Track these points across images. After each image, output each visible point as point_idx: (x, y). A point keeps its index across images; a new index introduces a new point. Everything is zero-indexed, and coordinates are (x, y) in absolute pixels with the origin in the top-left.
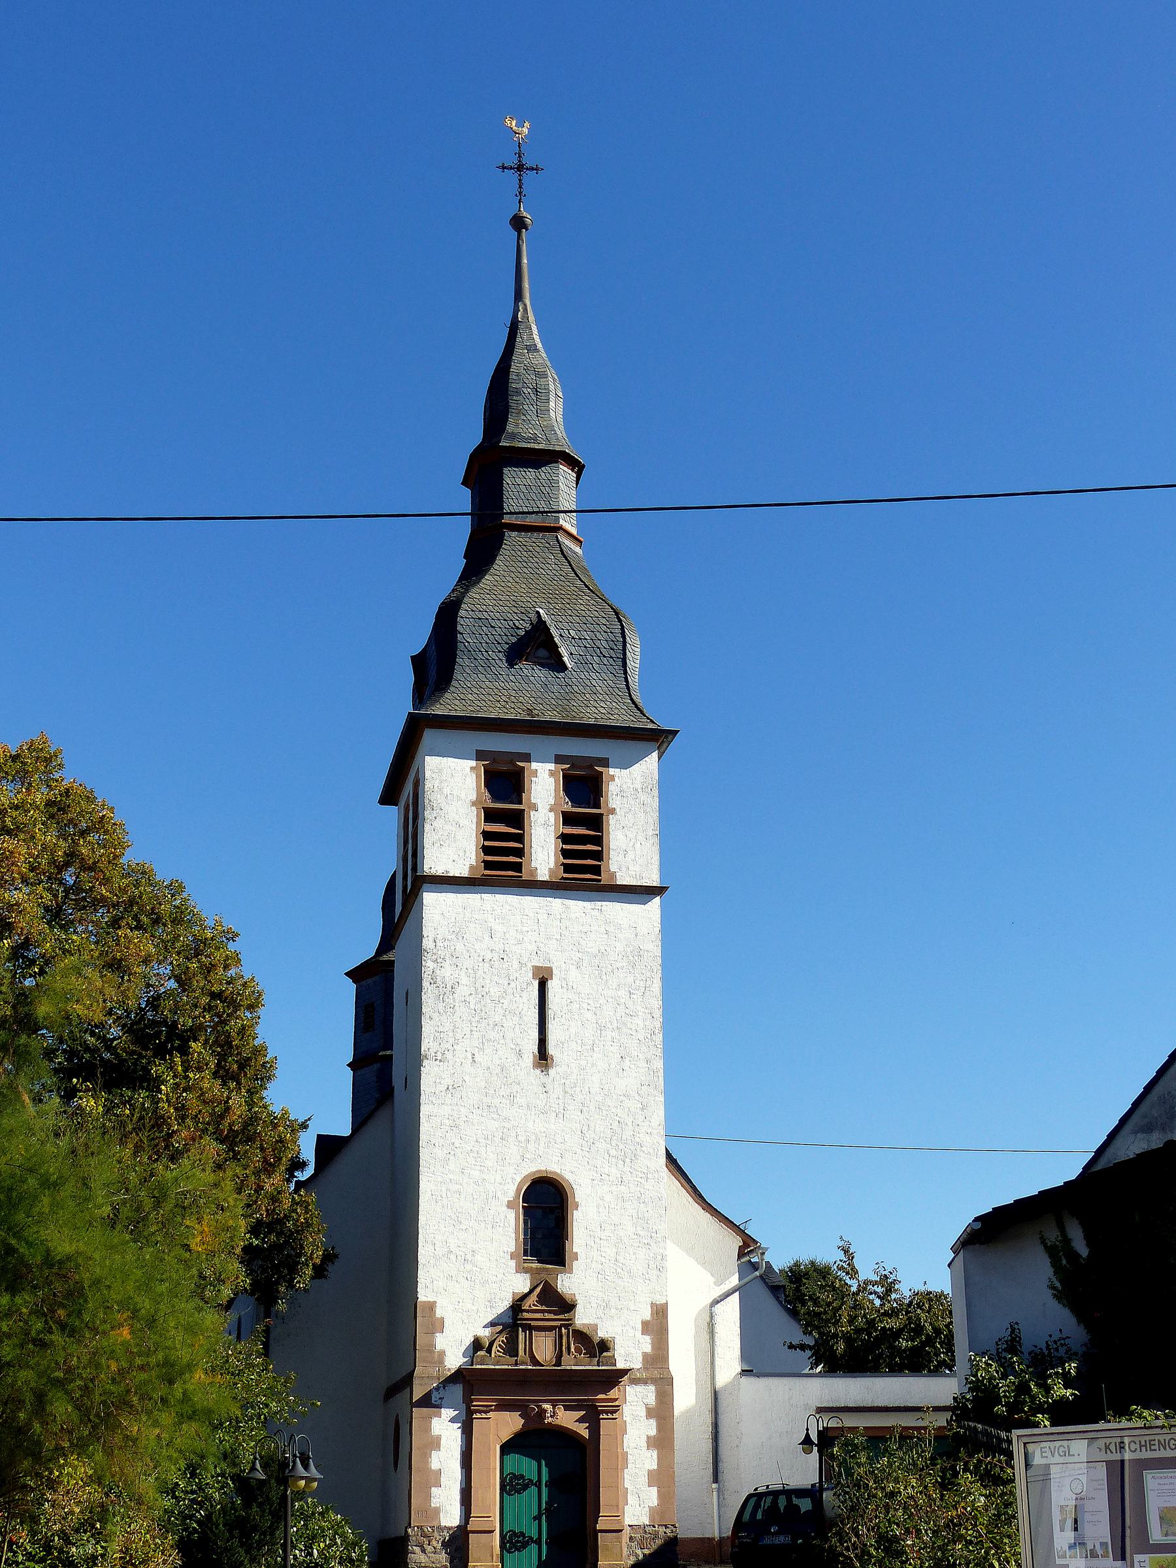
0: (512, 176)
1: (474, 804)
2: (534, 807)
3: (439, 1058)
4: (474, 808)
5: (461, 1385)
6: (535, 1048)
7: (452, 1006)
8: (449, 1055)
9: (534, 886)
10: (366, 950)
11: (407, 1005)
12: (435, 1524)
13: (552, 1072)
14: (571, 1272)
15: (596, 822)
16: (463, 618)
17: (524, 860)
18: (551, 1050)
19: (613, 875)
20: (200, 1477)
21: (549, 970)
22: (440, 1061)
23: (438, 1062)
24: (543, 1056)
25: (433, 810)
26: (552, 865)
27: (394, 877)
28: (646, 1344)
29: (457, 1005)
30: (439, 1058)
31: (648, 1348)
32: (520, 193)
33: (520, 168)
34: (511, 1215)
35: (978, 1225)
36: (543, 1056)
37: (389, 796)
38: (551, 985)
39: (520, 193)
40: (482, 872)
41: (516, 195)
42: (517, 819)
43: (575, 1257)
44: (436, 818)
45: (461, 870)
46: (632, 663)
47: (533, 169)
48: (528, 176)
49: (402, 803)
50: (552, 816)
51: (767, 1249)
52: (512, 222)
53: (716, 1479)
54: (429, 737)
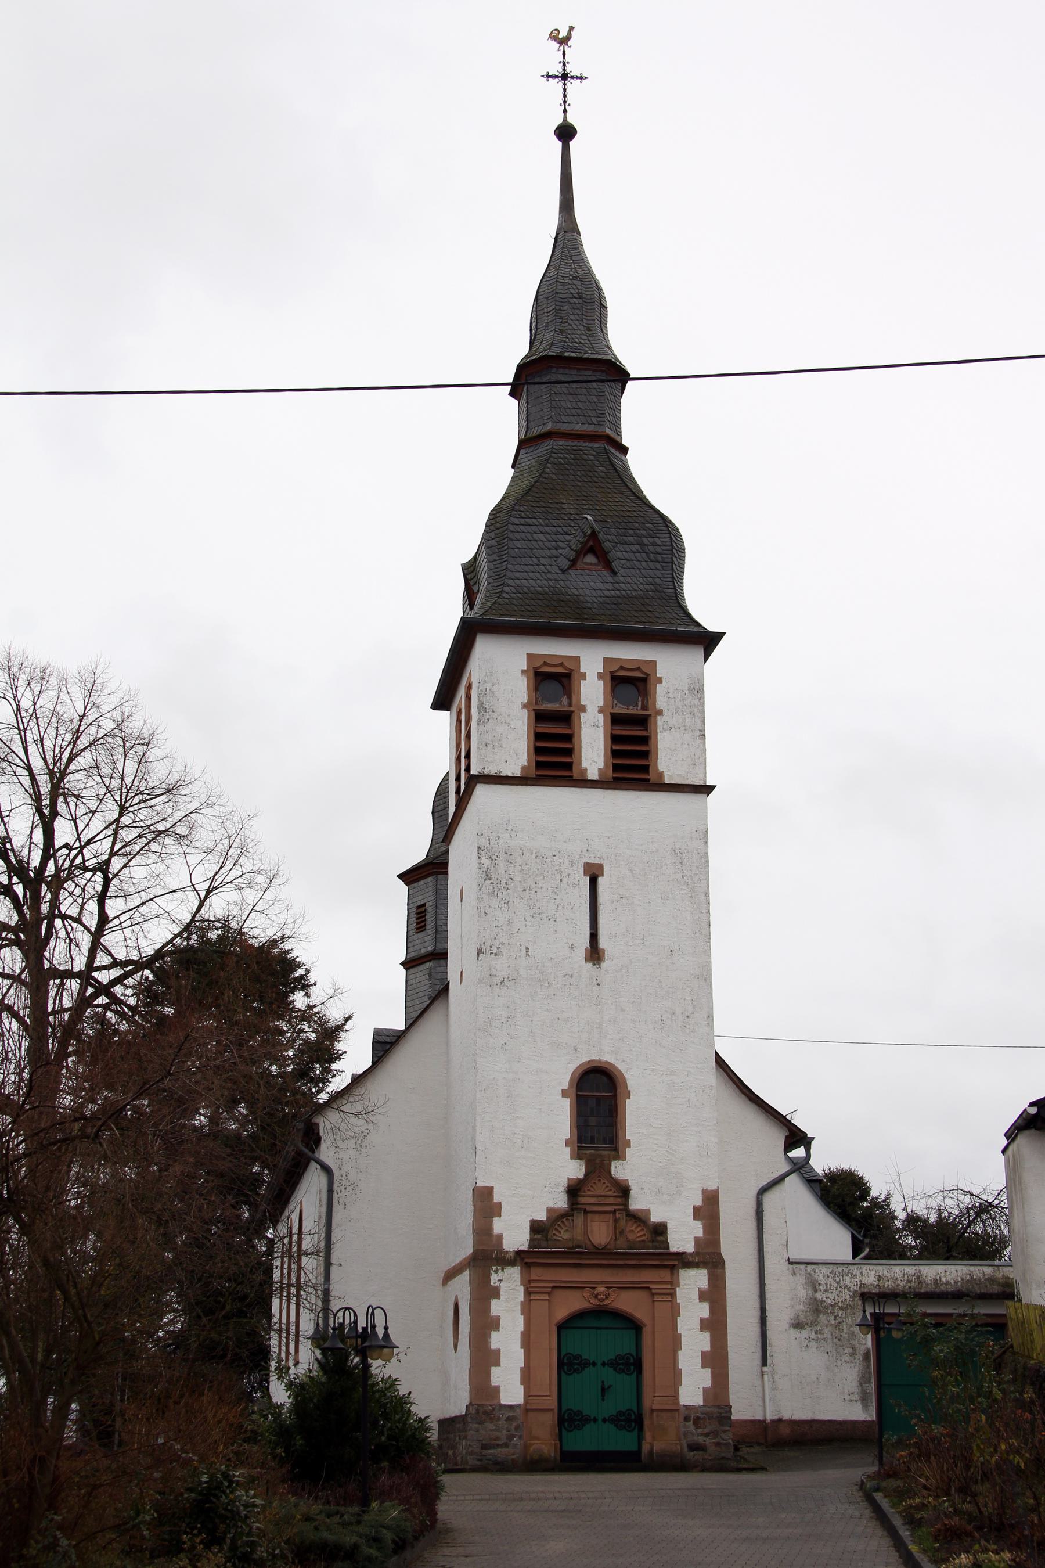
0: (556, 85)
1: (525, 706)
2: (583, 709)
3: (494, 952)
4: (526, 711)
5: (519, 1267)
6: (586, 943)
7: (506, 902)
8: (504, 949)
9: (584, 783)
10: (418, 854)
11: (462, 972)
12: (495, 1402)
13: (603, 965)
14: (625, 1159)
15: (643, 721)
16: (512, 540)
17: (575, 759)
18: (603, 943)
19: (661, 775)
20: (61, 791)
21: (600, 867)
22: (496, 955)
23: (493, 955)
24: (595, 954)
25: (486, 712)
26: (601, 765)
27: (446, 778)
28: (697, 1229)
29: (511, 900)
30: (494, 952)
31: (700, 1233)
32: (565, 102)
33: (565, 77)
34: (567, 1102)
35: (1033, 1110)
36: (595, 954)
37: (442, 701)
38: (601, 881)
39: (565, 102)
40: (533, 773)
41: (561, 105)
42: (567, 718)
43: (628, 1144)
44: (488, 720)
45: (514, 769)
46: (678, 568)
47: (577, 78)
48: (573, 86)
49: (455, 707)
50: (601, 717)
51: (813, 1139)
52: (557, 131)
53: (764, 1363)
54: (481, 791)
